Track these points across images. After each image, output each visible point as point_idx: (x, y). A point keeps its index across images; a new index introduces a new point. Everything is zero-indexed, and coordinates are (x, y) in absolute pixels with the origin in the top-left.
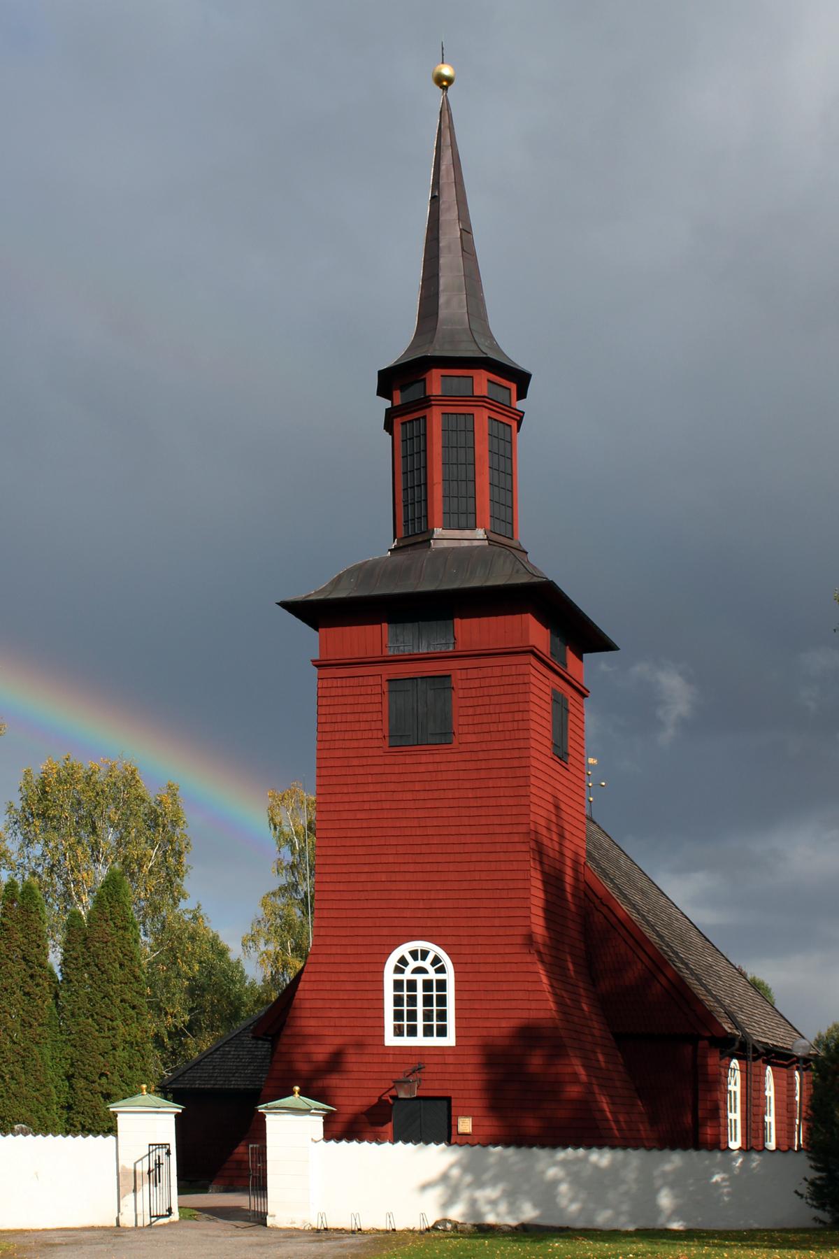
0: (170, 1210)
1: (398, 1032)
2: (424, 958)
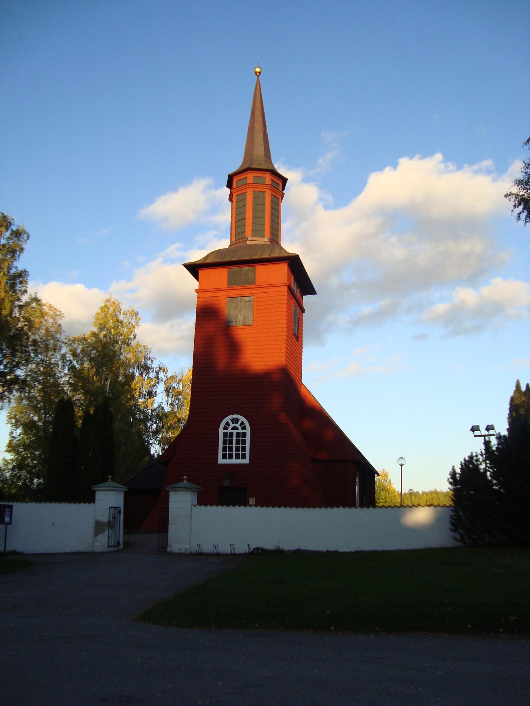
0: (119, 543)
1: (224, 457)
2: (237, 423)
